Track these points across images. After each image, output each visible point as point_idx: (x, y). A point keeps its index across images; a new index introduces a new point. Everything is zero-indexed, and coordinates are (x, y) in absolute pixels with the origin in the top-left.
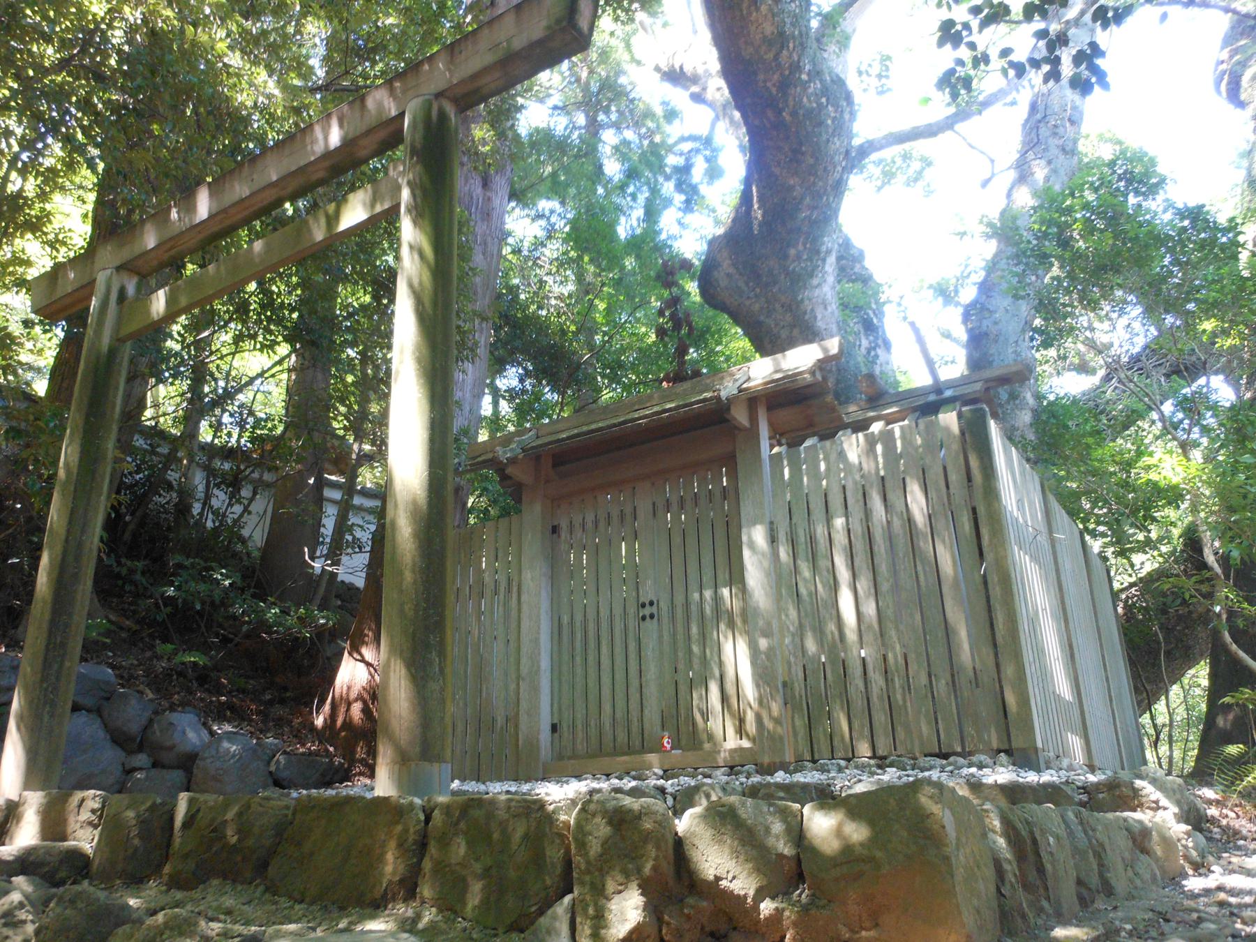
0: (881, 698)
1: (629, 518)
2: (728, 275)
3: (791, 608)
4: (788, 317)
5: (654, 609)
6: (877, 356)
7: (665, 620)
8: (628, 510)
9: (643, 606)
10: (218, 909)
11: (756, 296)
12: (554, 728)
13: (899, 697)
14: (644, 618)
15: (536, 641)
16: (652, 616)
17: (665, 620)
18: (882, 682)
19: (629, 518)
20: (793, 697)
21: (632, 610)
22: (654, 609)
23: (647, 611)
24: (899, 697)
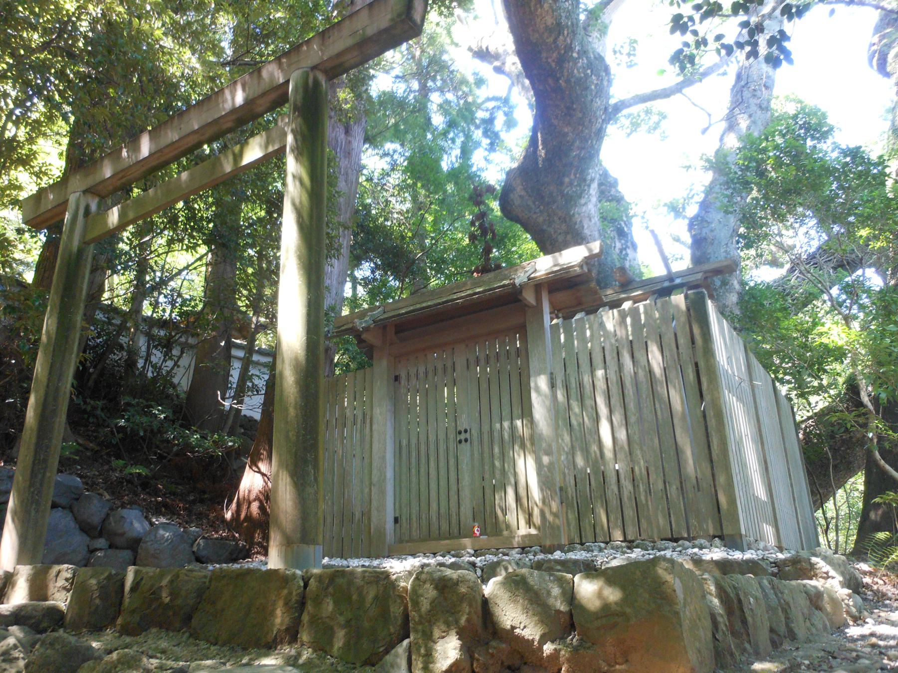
0: (630, 499)
1: (449, 370)
2: (521, 196)
4: (564, 227)
5: (468, 435)
6: (627, 255)
7: (476, 443)
8: (449, 364)
9: (460, 433)
11: (541, 211)
12: (396, 520)
13: (643, 498)
14: (460, 442)
15: (383, 458)
16: (466, 440)
17: (476, 443)
18: (630, 488)
19: (449, 370)
20: (567, 498)
21: (452, 436)
22: (468, 435)
23: (463, 437)
24: (643, 498)
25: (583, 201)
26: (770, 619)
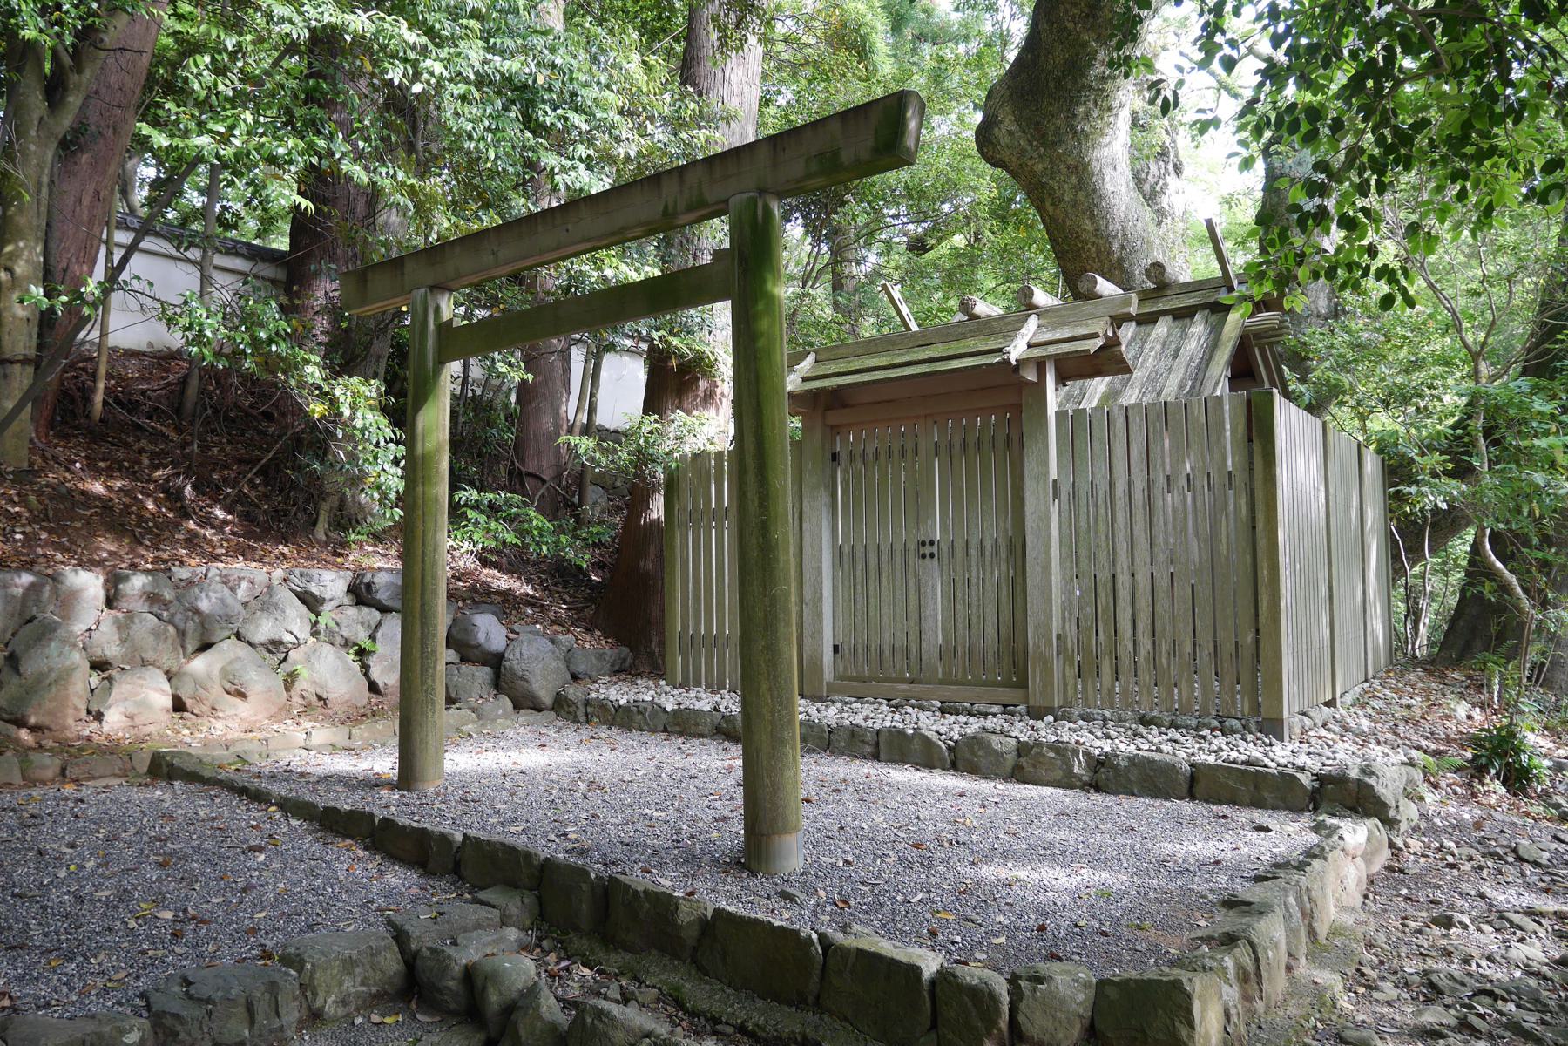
0: (1147, 660)
1: (909, 454)
2: (1010, 133)
3: (824, 515)
4: (1074, 180)
5: (935, 549)
6: (1166, 185)
7: (945, 561)
8: (910, 447)
9: (923, 544)
10: (1540, 591)
11: (1040, 156)
12: (836, 649)
13: (1164, 661)
14: (924, 556)
15: (819, 569)
16: (932, 555)
17: (945, 561)
18: (1149, 646)
19: (909, 454)
20: (1066, 648)
21: (912, 546)
22: (935, 549)
23: (927, 550)
24: (1164, 661)
25: (1105, 140)
26: (1288, 943)
